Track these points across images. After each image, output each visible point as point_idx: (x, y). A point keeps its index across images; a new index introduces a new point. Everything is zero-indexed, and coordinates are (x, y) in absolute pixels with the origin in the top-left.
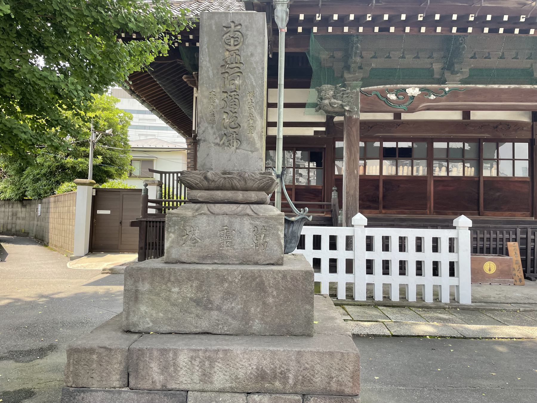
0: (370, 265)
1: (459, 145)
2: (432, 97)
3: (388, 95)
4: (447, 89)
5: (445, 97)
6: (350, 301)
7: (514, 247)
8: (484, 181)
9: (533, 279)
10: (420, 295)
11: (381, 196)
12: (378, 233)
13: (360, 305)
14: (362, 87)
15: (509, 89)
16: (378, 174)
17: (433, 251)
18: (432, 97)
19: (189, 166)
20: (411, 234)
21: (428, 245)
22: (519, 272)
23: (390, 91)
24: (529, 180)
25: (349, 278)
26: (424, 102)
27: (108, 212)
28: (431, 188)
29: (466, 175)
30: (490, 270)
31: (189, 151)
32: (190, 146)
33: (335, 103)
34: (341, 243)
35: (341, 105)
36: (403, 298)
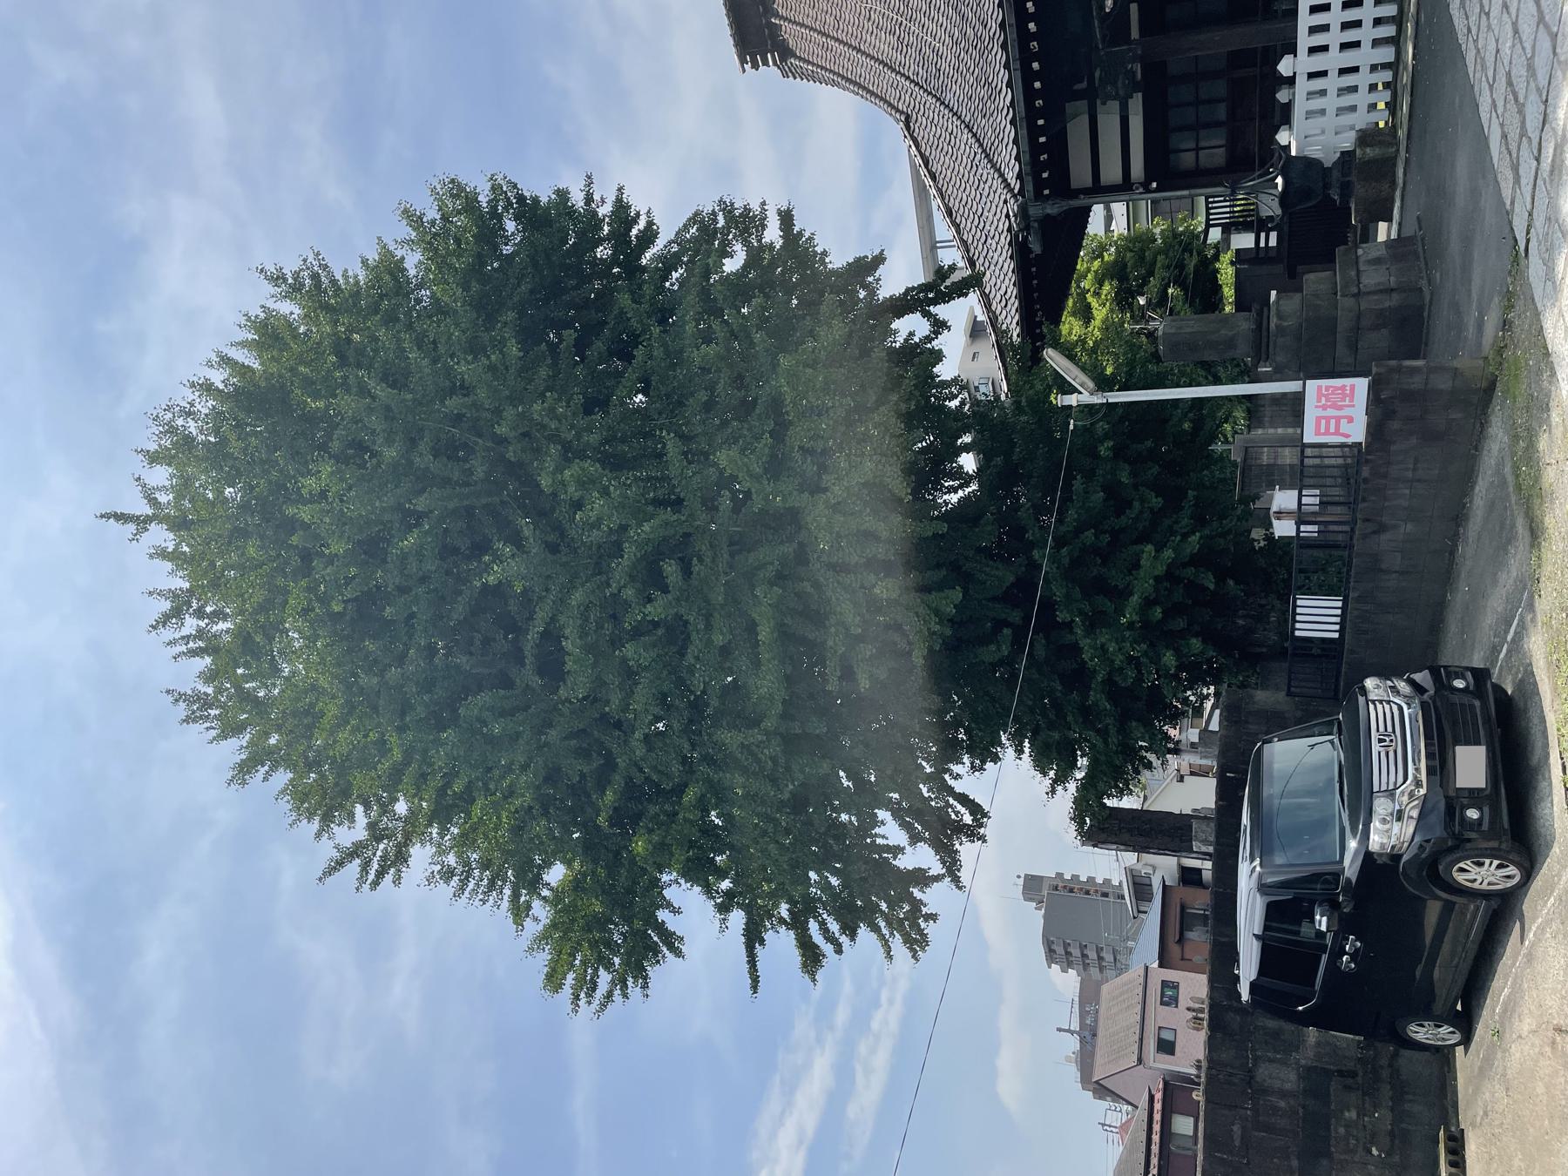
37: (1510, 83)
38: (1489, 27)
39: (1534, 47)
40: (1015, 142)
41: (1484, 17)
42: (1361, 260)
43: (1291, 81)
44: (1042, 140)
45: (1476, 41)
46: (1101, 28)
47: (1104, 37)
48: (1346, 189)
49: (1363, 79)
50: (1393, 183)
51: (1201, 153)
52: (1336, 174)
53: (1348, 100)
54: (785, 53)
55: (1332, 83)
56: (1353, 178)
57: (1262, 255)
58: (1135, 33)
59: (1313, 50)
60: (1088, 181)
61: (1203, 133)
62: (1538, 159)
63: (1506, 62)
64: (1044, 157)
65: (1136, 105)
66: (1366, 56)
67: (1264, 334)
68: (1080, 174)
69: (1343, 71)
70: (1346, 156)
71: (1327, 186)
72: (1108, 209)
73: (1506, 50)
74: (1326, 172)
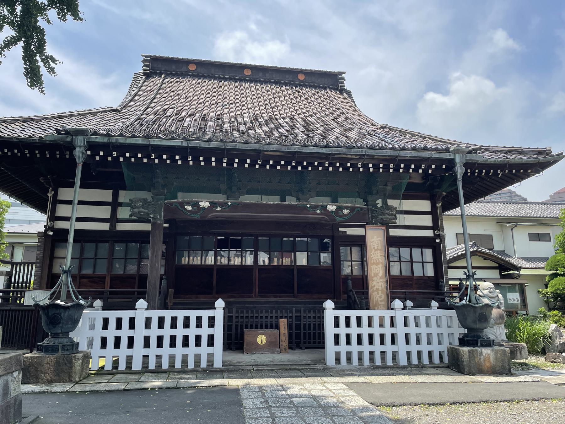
1: (305, 239)
2: (219, 209)
3: (186, 207)
4: (230, 204)
5: (227, 209)
6: (128, 371)
7: (283, 323)
8: (297, 269)
9: (303, 348)
10: (197, 362)
11: (214, 282)
12: (342, 314)
13: (122, 373)
14: (165, 200)
15: (273, 204)
16: (213, 263)
17: (346, 327)
18: (219, 209)
19: (39, 257)
22: (285, 343)
23: (188, 204)
24: (331, 268)
25: (129, 352)
26: (212, 213)
28: (256, 274)
29: (284, 264)
30: (262, 342)
31: (39, 244)
32: (40, 240)
33: (142, 212)
35: (147, 213)
36: (159, 366)
43: (390, 308)
48: (47, 349)
50: (50, 382)
51: (93, 256)
52: (65, 341)
54: (148, 76)
56: (60, 353)
60: (61, 197)
71: (56, 335)
72: (10, 221)
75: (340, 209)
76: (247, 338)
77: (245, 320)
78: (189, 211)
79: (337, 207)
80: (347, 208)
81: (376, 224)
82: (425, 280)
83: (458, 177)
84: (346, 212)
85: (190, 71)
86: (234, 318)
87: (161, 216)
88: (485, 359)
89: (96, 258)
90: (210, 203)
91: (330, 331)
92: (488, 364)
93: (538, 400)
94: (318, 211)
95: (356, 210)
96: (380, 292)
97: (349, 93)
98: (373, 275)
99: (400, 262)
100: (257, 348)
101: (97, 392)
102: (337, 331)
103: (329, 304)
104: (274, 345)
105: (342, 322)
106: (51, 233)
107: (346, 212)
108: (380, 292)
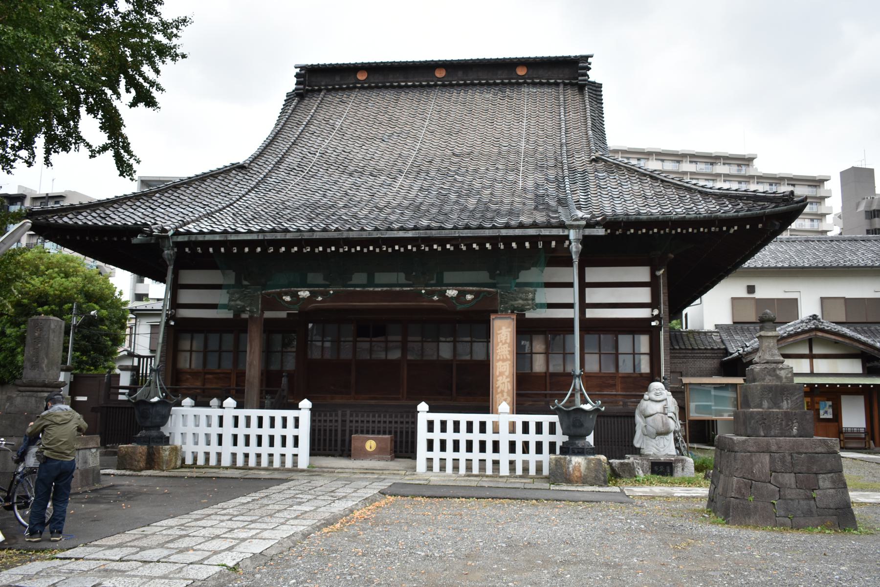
0: (512, 445)
2: (320, 299)
12: (437, 417)
20: (463, 418)
21: (266, 422)
23: (286, 294)
27: (85, 399)
34: (489, 427)
37: (181, 537)
38: (222, 521)
39: (199, 550)
40: (212, 232)
41: (229, 517)
42: (87, 452)
44: (211, 250)
45: (216, 514)
46: (274, 293)
47: (269, 294)
48: (140, 441)
49: (214, 449)
53: (202, 440)
55: (215, 430)
57: (113, 390)
58: (268, 314)
59: (236, 418)
61: (201, 355)
62: (121, 560)
63: (194, 534)
64: (199, 250)
65: (229, 315)
66: (227, 448)
67: (40, 389)
68: (189, 276)
69: (220, 436)
70: (166, 440)
73: (203, 532)
74: (158, 427)
75: (462, 294)
76: (355, 444)
77: (371, 425)
78: (287, 302)
79: (459, 291)
80: (470, 292)
81: (505, 311)
82: (601, 377)
83: (574, 257)
84: (469, 297)
85: (359, 81)
86: (348, 422)
87: (258, 309)
88: (575, 467)
89: (220, 351)
90: (310, 292)
91: (422, 435)
92: (577, 474)
93: (560, 501)
94: (436, 298)
95: (481, 296)
96: (505, 394)
97: (596, 88)
98: (498, 374)
99: (600, 354)
100: (365, 455)
101: (176, 477)
102: (430, 436)
103: (423, 407)
104: (379, 453)
105: (437, 426)
106: (172, 323)
107: (469, 297)
108: (505, 394)
